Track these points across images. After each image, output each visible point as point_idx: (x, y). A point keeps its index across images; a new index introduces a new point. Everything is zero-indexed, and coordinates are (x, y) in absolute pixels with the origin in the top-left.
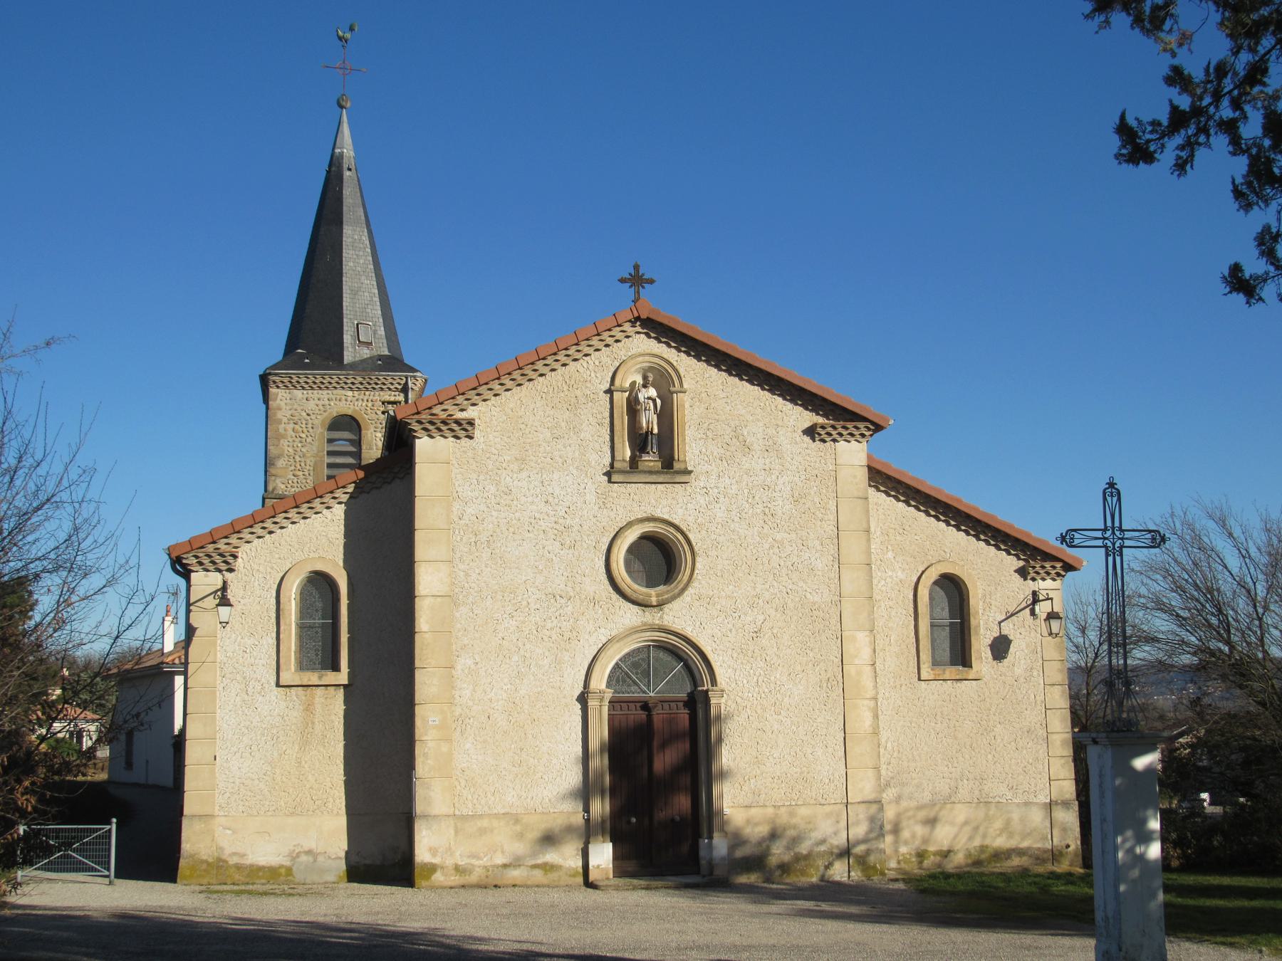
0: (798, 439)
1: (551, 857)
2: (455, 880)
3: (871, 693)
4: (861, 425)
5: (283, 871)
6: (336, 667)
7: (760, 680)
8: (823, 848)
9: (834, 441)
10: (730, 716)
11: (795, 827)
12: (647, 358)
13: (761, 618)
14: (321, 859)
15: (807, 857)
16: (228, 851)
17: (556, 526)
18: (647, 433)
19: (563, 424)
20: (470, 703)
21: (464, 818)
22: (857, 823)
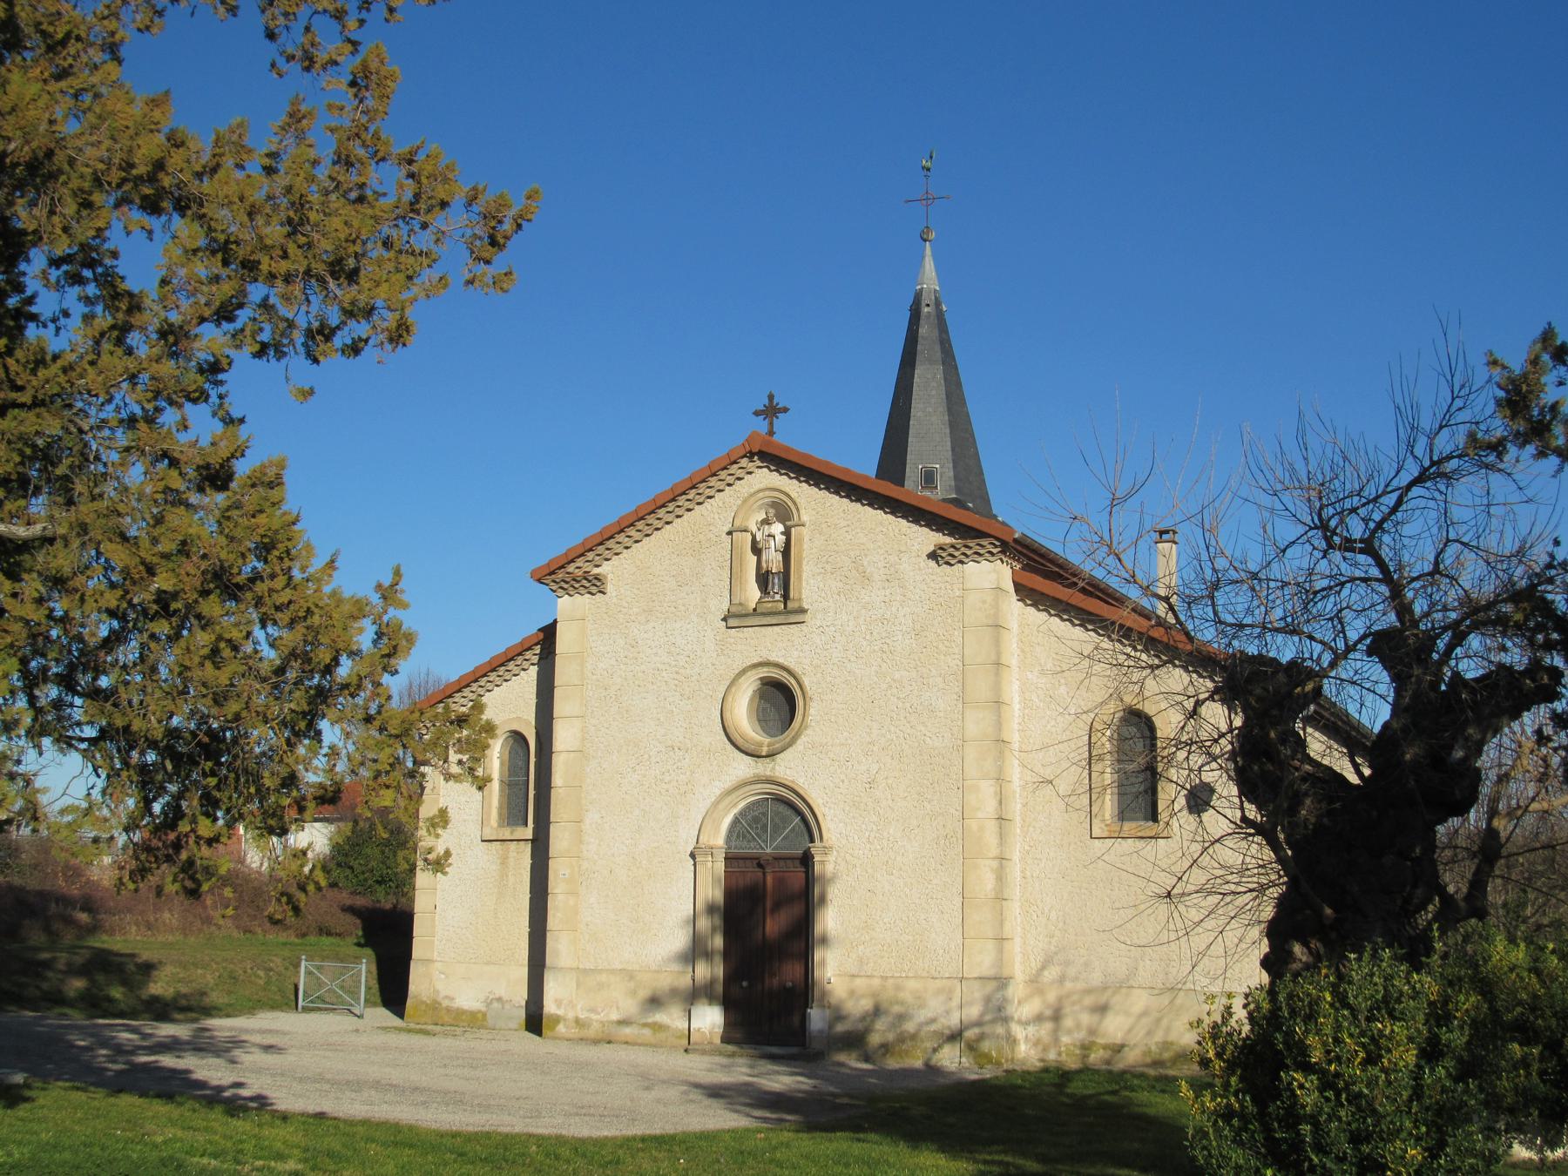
0: (922, 564)
1: (660, 1017)
2: (574, 1032)
3: (994, 852)
4: (984, 542)
5: (480, 1016)
6: (526, 824)
7: (872, 835)
8: (933, 1027)
9: (961, 562)
10: (832, 880)
11: (902, 1003)
12: (767, 493)
13: (875, 767)
14: (507, 1006)
15: (914, 1037)
16: (442, 994)
17: (676, 676)
18: (768, 572)
19: (687, 571)
20: (596, 857)
21: (586, 972)
22: (971, 1004)
